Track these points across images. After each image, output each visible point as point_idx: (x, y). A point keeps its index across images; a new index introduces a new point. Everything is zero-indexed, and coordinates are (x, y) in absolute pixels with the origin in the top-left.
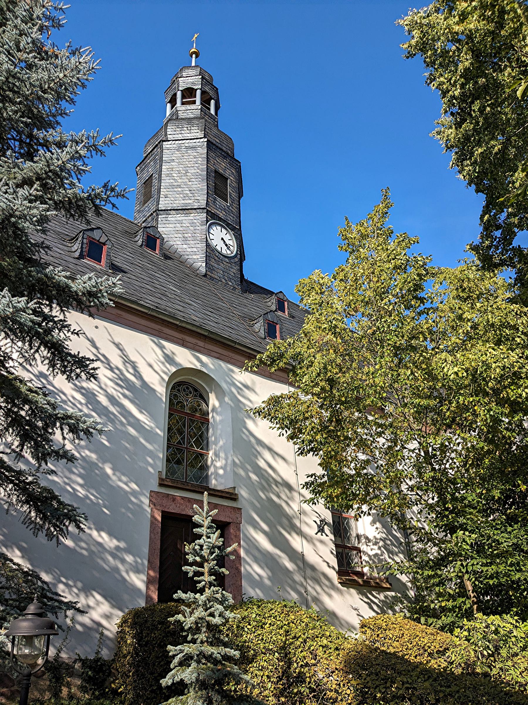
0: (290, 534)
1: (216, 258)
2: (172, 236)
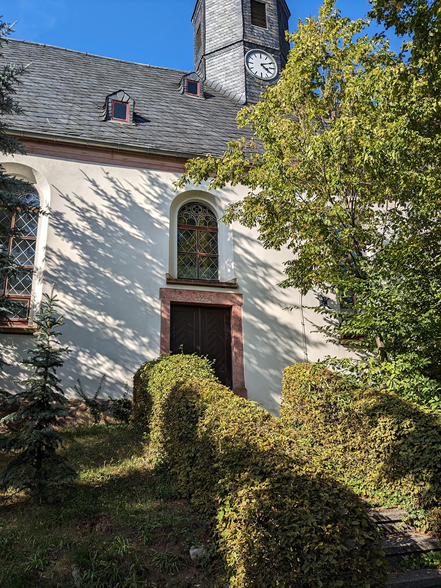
0: (264, 302)
1: (257, 85)
2: (217, 75)
